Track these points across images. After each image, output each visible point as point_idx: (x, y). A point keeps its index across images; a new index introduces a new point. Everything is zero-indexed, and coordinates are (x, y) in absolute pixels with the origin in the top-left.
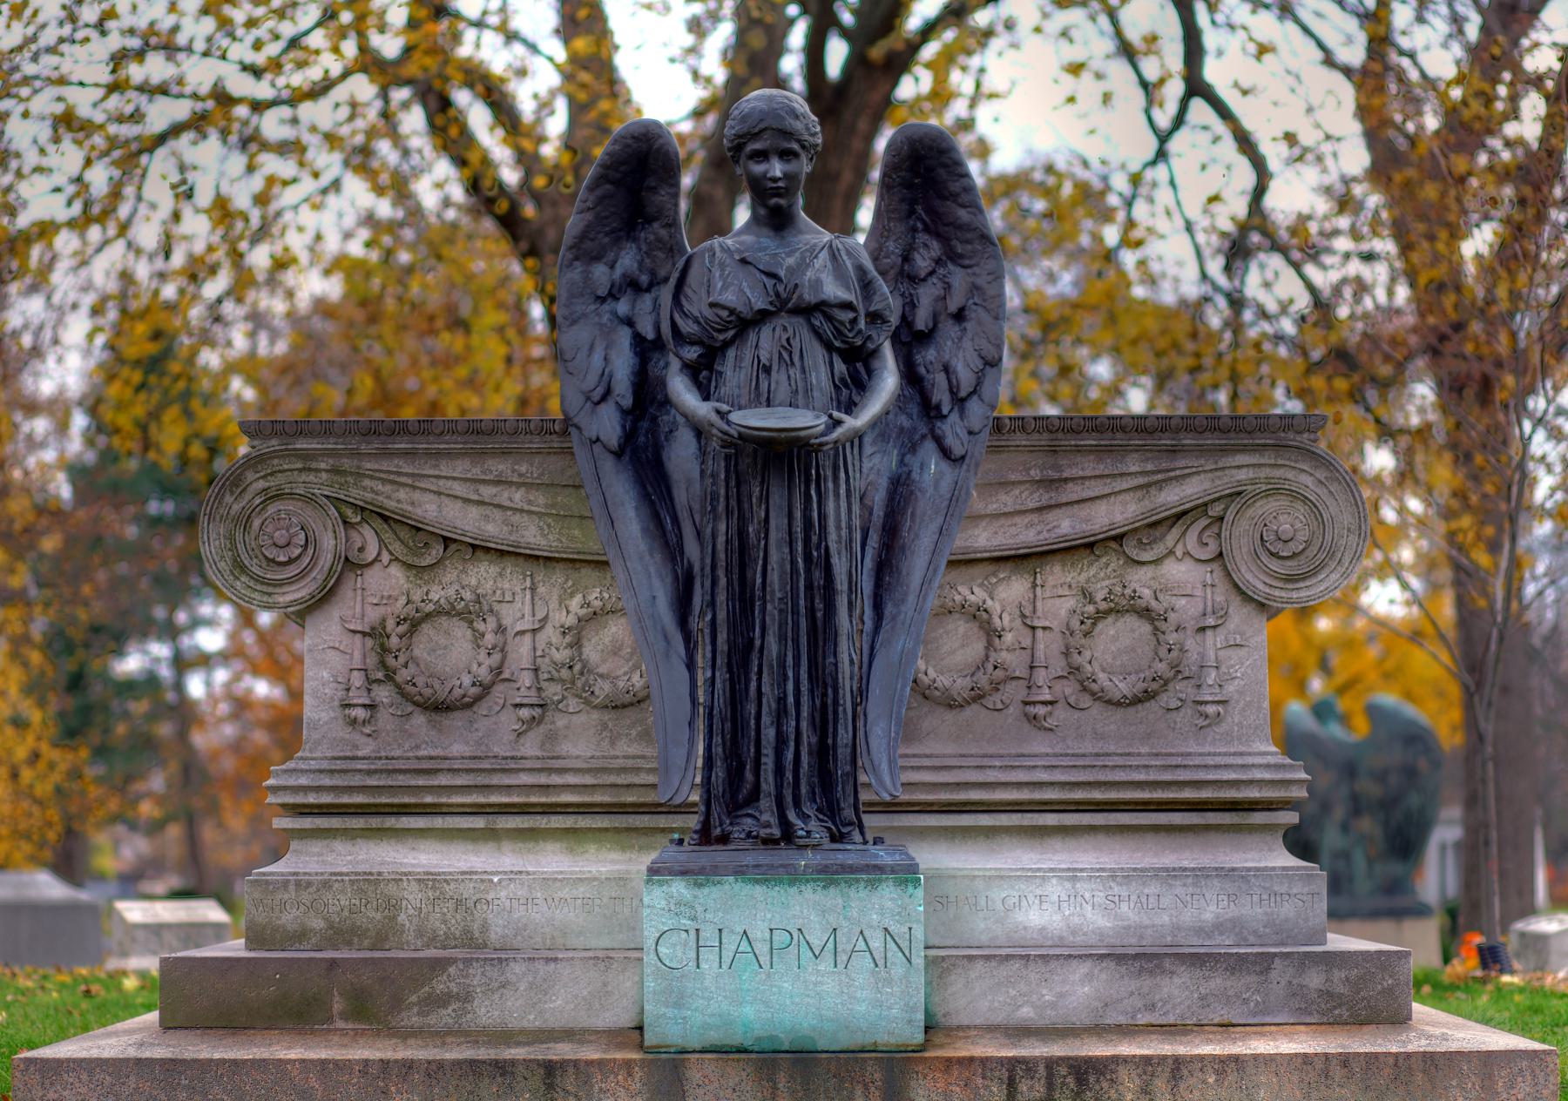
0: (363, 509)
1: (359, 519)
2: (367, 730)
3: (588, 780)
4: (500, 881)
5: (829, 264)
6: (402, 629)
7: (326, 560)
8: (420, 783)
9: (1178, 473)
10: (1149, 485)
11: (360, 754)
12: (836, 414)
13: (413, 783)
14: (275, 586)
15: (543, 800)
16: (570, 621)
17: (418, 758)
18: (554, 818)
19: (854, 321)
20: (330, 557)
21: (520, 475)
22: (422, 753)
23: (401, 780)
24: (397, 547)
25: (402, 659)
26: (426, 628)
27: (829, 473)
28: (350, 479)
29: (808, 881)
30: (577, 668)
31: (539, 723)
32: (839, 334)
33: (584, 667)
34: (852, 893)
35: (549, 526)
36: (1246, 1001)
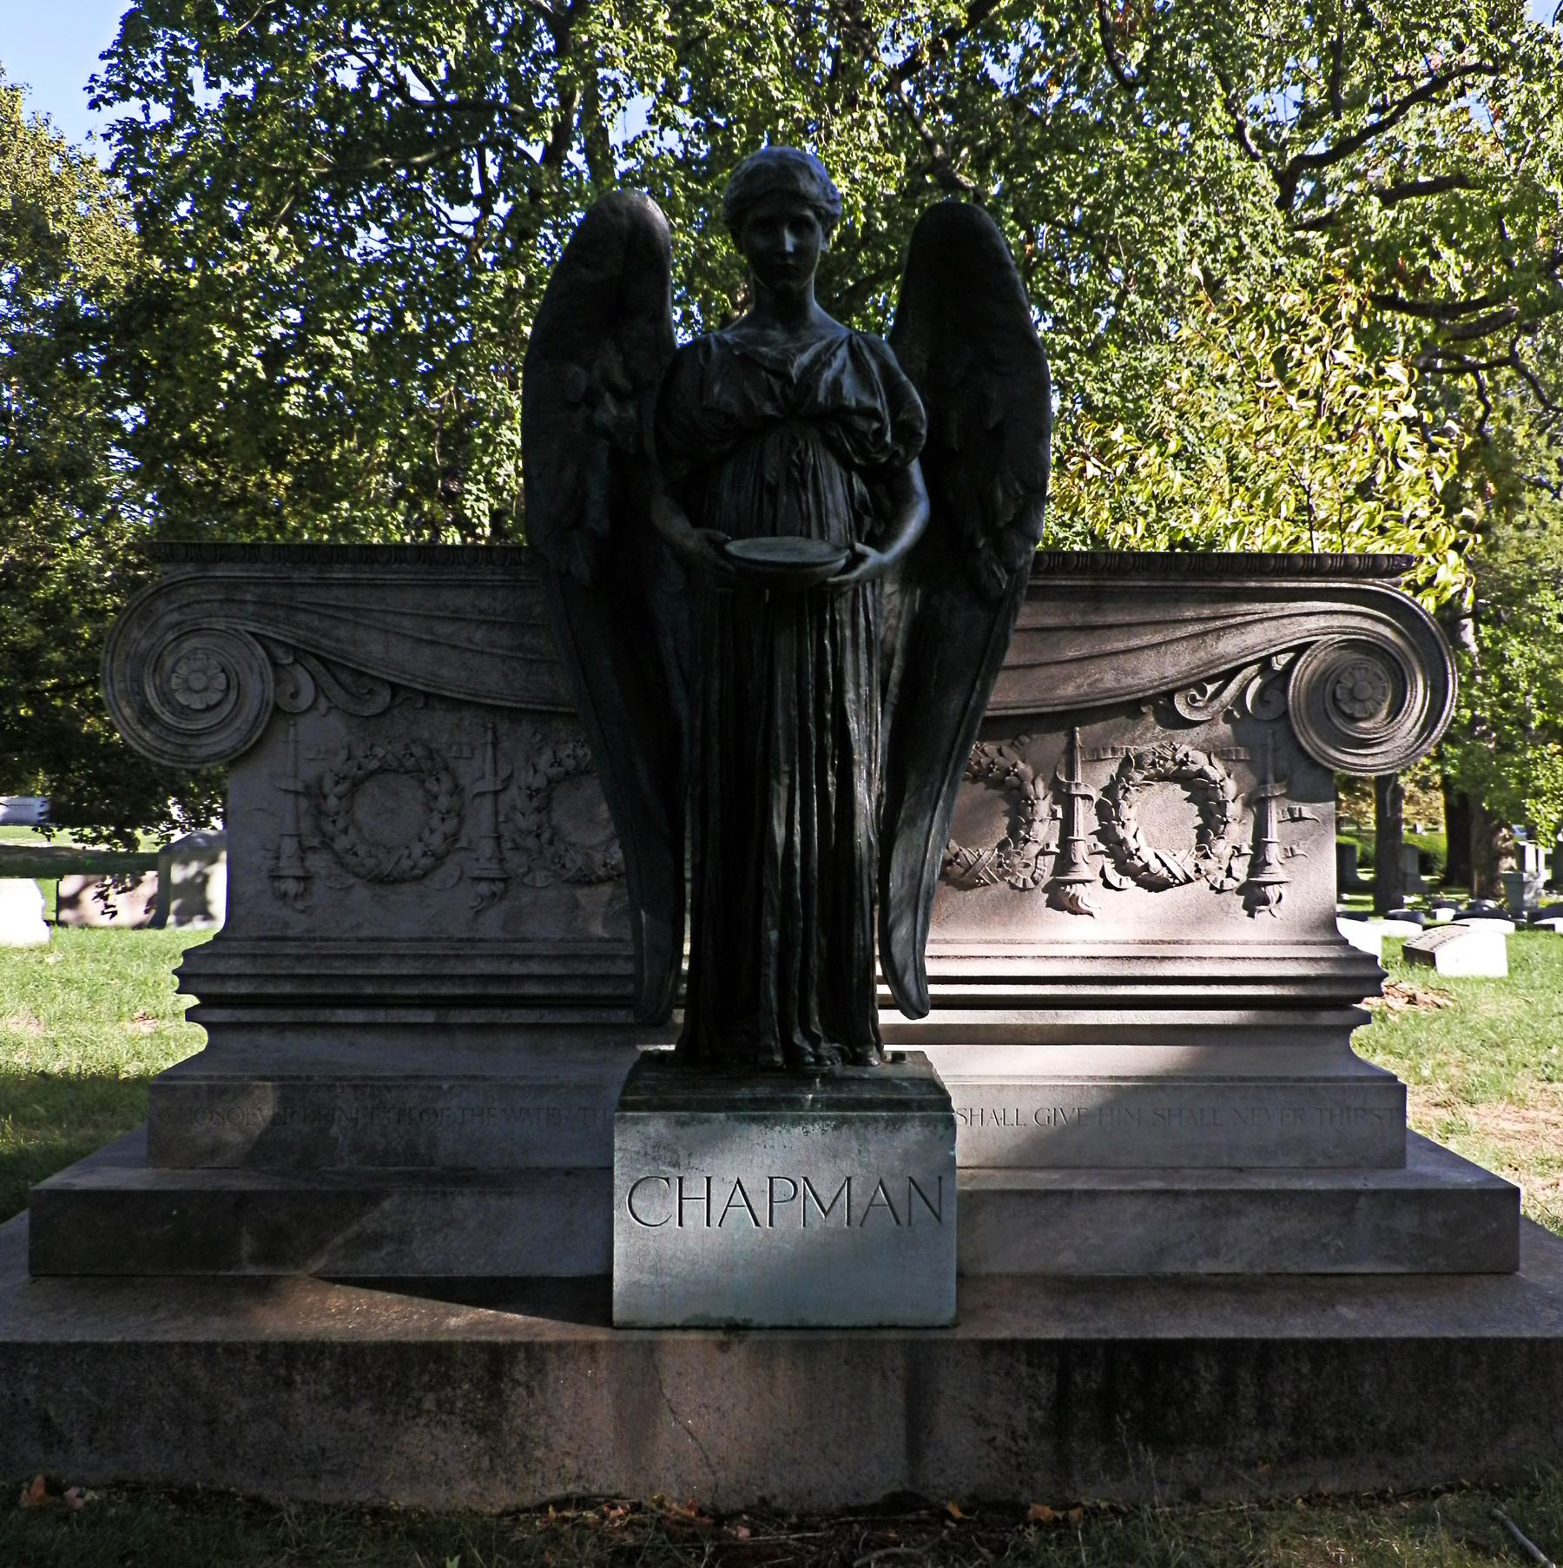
0: (295, 649)
1: (291, 660)
2: (300, 905)
3: (556, 969)
4: (451, 1088)
5: (849, 364)
6: (341, 788)
7: (251, 706)
8: (359, 971)
9: (1239, 619)
10: (1205, 633)
11: (291, 933)
12: (859, 547)
13: (350, 972)
14: (191, 736)
15: (503, 991)
16: (539, 782)
17: (360, 940)
18: (516, 1012)
19: (880, 433)
20: (256, 703)
21: (481, 612)
22: (364, 933)
23: (338, 968)
24: (336, 692)
25: (341, 824)
26: (370, 787)
27: (847, 617)
28: (281, 613)
29: (815, 1120)
30: (546, 836)
31: (501, 898)
32: (860, 449)
33: (553, 836)
34: (870, 1133)
35: (514, 670)
36: (1325, 1247)
